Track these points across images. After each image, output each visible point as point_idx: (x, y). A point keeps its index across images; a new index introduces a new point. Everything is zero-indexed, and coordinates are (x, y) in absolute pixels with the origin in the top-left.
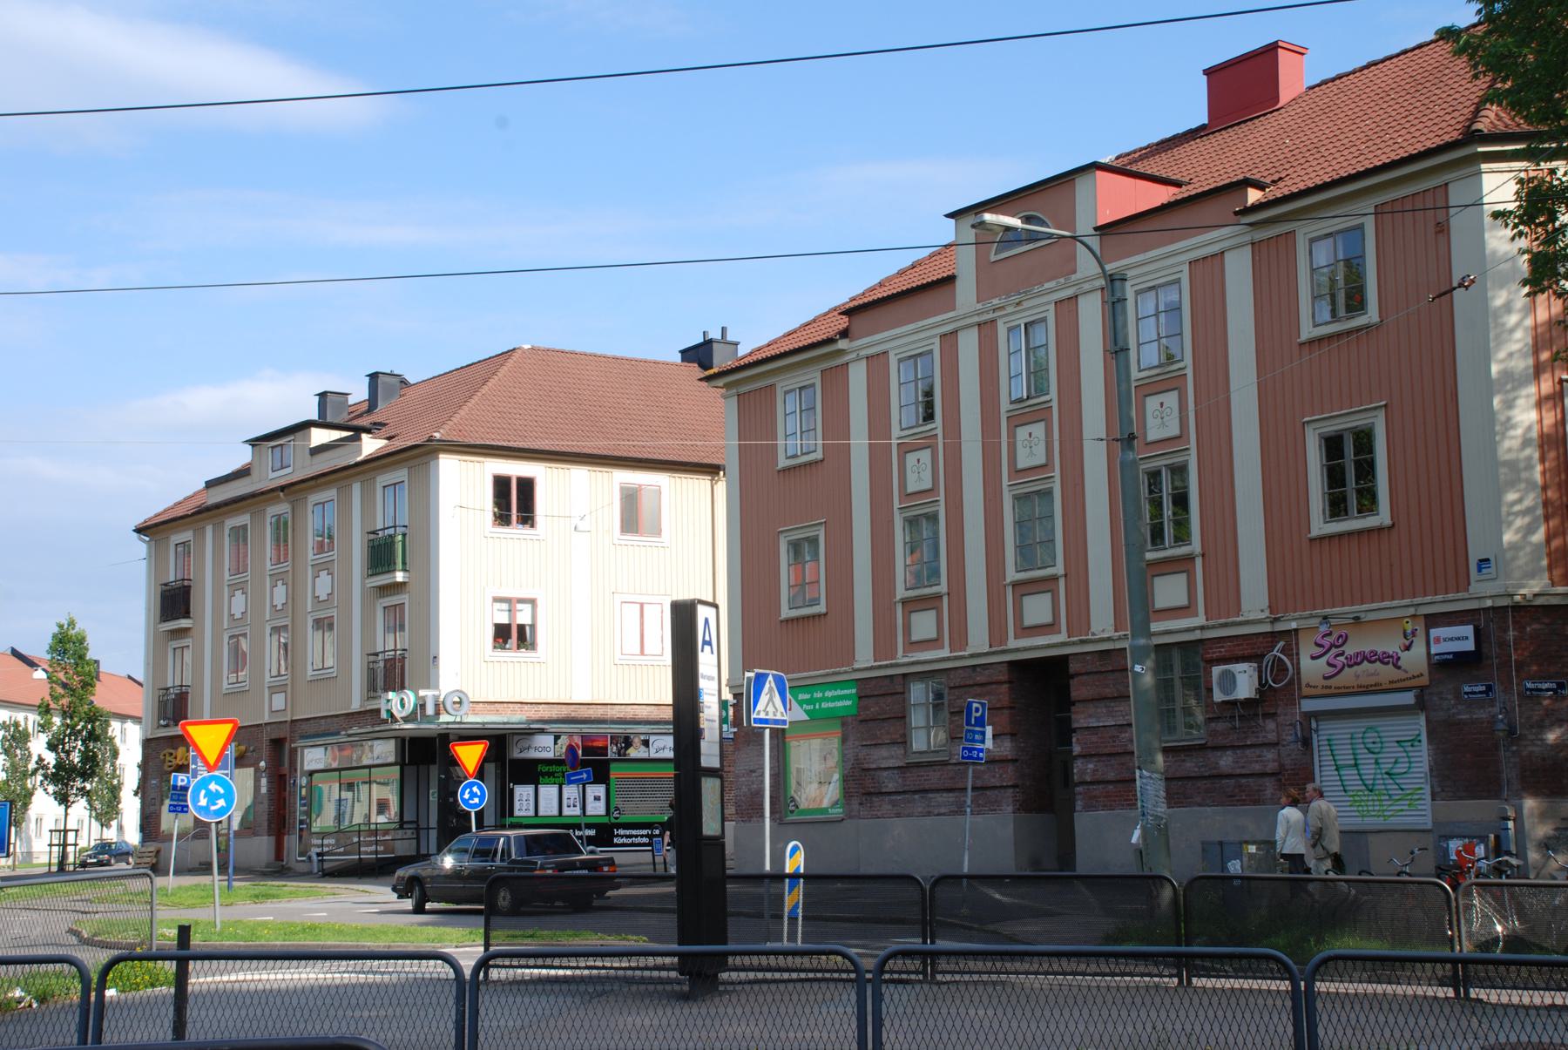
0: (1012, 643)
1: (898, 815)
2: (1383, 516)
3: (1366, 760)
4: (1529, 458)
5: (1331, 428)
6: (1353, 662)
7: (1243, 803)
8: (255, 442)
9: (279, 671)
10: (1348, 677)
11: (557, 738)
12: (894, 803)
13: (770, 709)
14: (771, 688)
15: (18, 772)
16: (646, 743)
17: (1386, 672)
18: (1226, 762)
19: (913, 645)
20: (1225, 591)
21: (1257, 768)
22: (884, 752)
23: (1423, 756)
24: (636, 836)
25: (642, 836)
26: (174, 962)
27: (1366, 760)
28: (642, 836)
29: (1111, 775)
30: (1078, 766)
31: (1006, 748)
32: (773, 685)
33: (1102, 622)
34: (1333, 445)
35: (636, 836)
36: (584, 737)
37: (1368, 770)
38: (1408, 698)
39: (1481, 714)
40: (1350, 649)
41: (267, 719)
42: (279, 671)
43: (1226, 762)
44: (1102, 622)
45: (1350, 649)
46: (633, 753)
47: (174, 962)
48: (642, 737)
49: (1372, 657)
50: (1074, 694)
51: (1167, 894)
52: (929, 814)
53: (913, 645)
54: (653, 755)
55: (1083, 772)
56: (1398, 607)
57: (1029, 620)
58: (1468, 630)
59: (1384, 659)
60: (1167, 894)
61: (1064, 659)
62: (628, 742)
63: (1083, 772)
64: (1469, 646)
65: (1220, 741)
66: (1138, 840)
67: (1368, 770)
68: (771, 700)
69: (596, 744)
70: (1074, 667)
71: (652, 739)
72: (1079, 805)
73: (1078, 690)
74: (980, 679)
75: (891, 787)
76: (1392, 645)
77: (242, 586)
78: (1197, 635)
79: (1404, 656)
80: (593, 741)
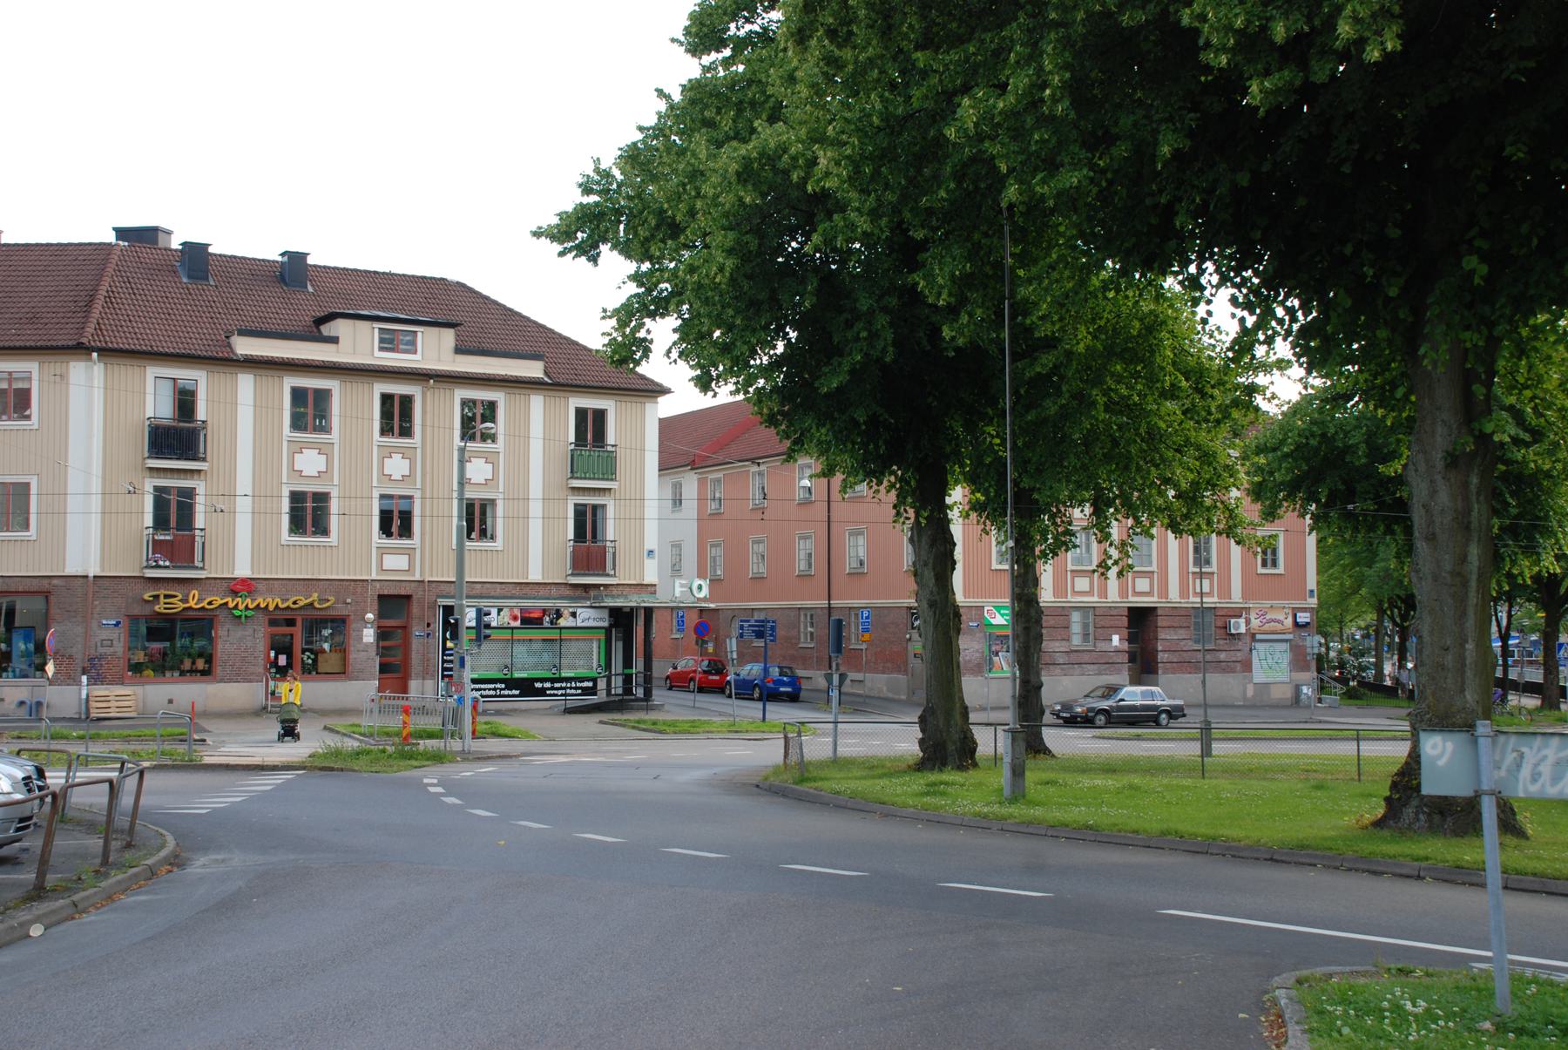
0: (1070, 599)
1: (1065, 675)
2: (1280, 570)
3: (1269, 657)
4: (483, 421)
7: (1228, 672)
8: (121, 233)
10: (1267, 627)
11: (500, 611)
12: (1062, 669)
16: (574, 615)
17: (1279, 626)
18: (1222, 656)
19: (1075, 593)
20: (1225, 590)
21: (1234, 659)
22: (1057, 644)
24: (485, 690)
25: (490, 689)
27: (1269, 657)
28: (490, 689)
29: (1175, 660)
30: (1160, 655)
31: (1126, 646)
33: (1174, 595)
35: (485, 690)
36: (522, 610)
37: (1270, 661)
38: (1258, 637)
40: (1268, 617)
41: (374, 576)
43: (1222, 656)
45: (1268, 617)
46: (562, 622)
48: (571, 610)
50: (1159, 624)
52: (1083, 675)
53: (1075, 593)
54: (579, 624)
55: (1162, 658)
58: (1308, 614)
59: (1279, 621)
61: (1155, 609)
62: (559, 614)
63: (1162, 658)
65: (1221, 648)
67: (1270, 661)
69: (532, 615)
70: (1159, 612)
71: (579, 611)
72: (1160, 672)
73: (1161, 622)
74: (1112, 613)
75: (1061, 661)
76: (1281, 617)
77: (486, 455)
78: (1213, 606)
80: (530, 613)
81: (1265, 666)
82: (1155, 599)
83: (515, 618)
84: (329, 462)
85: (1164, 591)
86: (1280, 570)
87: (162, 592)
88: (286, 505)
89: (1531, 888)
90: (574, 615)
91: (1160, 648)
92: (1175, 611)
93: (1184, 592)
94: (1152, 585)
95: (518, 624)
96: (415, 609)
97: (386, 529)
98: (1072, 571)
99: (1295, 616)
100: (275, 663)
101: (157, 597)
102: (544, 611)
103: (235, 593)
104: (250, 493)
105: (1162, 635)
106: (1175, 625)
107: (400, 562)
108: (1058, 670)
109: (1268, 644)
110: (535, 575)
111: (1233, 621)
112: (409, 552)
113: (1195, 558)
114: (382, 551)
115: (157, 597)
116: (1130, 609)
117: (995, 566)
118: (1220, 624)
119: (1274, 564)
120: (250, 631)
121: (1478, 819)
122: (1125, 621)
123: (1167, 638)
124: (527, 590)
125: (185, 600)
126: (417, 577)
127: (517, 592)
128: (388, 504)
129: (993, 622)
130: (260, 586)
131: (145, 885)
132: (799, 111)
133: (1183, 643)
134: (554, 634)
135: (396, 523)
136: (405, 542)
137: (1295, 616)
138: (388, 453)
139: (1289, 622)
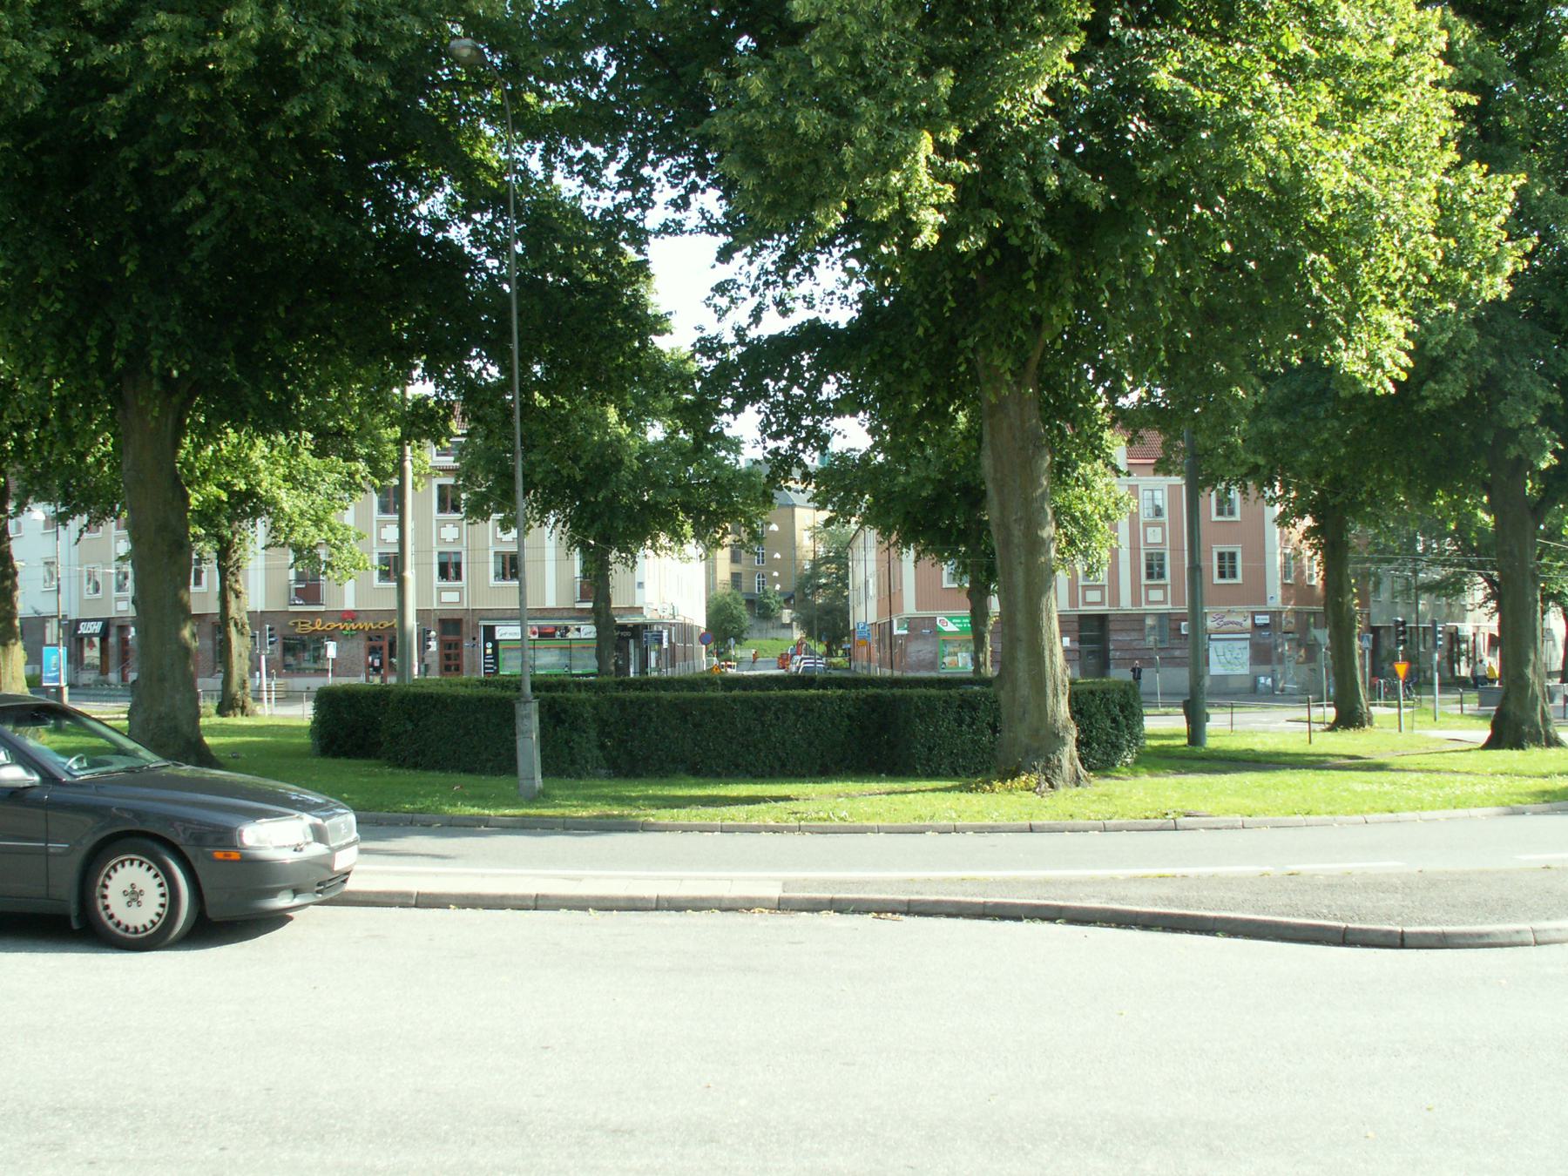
0: (1081, 608)
2: (1239, 580)
9: (516, 649)
10: (1225, 628)
15: (84, 21)
16: (579, 630)
17: (1238, 628)
18: (1177, 653)
19: (1148, 602)
26: (397, 550)
31: (1076, 646)
33: (1126, 603)
34: (1221, 556)
36: (539, 627)
37: (1229, 656)
38: (1213, 636)
40: (1225, 620)
41: (435, 607)
42: (516, 649)
45: (1225, 620)
46: (570, 635)
47: (397, 550)
51: (1107, 384)
53: (1086, 603)
57: (1088, 600)
60: (1107, 384)
62: (567, 629)
66: (1151, 747)
67: (1229, 656)
70: (1110, 618)
73: (1112, 626)
76: (1239, 619)
81: (1224, 661)
82: (1107, 607)
83: (534, 633)
84: (379, 533)
85: (1115, 599)
86: (1239, 580)
87: (299, 620)
88: (436, 561)
90: (579, 630)
91: (1111, 647)
92: (1127, 617)
93: (1136, 600)
94: (1103, 596)
95: (536, 637)
96: (464, 629)
97: (444, 573)
99: (1253, 619)
100: (372, 665)
101: (296, 623)
102: (556, 628)
103: (343, 620)
105: (1114, 637)
107: (450, 597)
109: (1226, 643)
110: (551, 603)
112: (459, 590)
114: (440, 590)
115: (296, 623)
116: (1081, 616)
117: (946, 585)
118: (1174, 626)
119: (1234, 575)
120: (355, 644)
122: (1076, 626)
123: (73, 682)
124: (545, 614)
125: (313, 625)
126: (465, 607)
127: (538, 614)
128: (445, 558)
129: (945, 629)
130: (362, 615)
132: (1403, 182)
133: (1135, 643)
134: (566, 644)
135: (452, 572)
136: (458, 583)
137: (1253, 619)
138: (442, 523)
139: (1248, 623)
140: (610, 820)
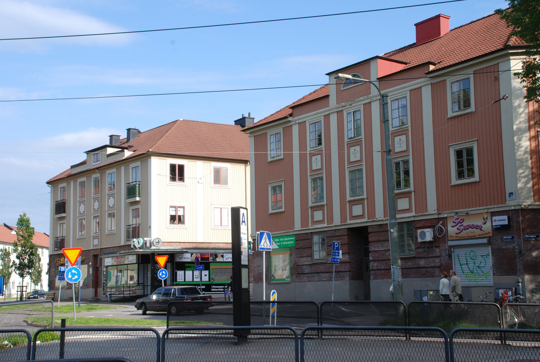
0: (349, 222)
1: (309, 281)
2: (476, 178)
3: (471, 262)
5: (458, 147)
6: (466, 228)
7: (428, 277)
9: (96, 231)
10: (464, 233)
12: (308, 277)
13: (265, 244)
14: (265, 237)
16: (222, 256)
17: (477, 232)
18: (422, 263)
19: (314, 222)
20: (422, 204)
21: (433, 265)
22: (304, 259)
23: (490, 261)
24: (219, 288)
25: (221, 288)
26: (60, 332)
27: (471, 262)
28: (221, 288)
29: (383, 267)
30: (371, 264)
31: (347, 258)
32: (266, 236)
33: (380, 214)
34: (459, 153)
35: (219, 288)
36: (201, 254)
37: (471, 265)
38: (485, 241)
39: (510, 246)
40: (465, 224)
41: (92, 248)
42: (96, 231)
43: (422, 263)
44: (380, 214)
45: (465, 224)
46: (218, 260)
47: (60, 332)
48: (221, 254)
49: (472, 227)
50: (370, 239)
52: (320, 281)
53: (314, 222)
55: (373, 266)
56: (481, 209)
57: (354, 214)
58: (506, 217)
59: (477, 227)
61: (366, 227)
62: (216, 256)
63: (373, 266)
64: (506, 223)
65: (420, 255)
67: (471, 265)
68: (265, 241)
69: (205, 256)
70: (370, 230)
72: (372, 277)
73: (371, 238)
74: (337, 234)
75: (307, 271)
76: (479, 223)
78: (412, 219)
79: (484, 226)
80: (204, 255)
89: (142, 327)
98: (350, 202)
104: (380, 150)
106: (382, 238)
108: (305, 278)
111: (419, 231)
113: (472, 155)
121: (81, 299)
131: (31, 295)
140: (183, 321)
